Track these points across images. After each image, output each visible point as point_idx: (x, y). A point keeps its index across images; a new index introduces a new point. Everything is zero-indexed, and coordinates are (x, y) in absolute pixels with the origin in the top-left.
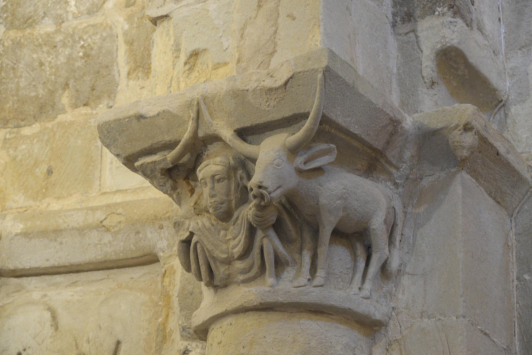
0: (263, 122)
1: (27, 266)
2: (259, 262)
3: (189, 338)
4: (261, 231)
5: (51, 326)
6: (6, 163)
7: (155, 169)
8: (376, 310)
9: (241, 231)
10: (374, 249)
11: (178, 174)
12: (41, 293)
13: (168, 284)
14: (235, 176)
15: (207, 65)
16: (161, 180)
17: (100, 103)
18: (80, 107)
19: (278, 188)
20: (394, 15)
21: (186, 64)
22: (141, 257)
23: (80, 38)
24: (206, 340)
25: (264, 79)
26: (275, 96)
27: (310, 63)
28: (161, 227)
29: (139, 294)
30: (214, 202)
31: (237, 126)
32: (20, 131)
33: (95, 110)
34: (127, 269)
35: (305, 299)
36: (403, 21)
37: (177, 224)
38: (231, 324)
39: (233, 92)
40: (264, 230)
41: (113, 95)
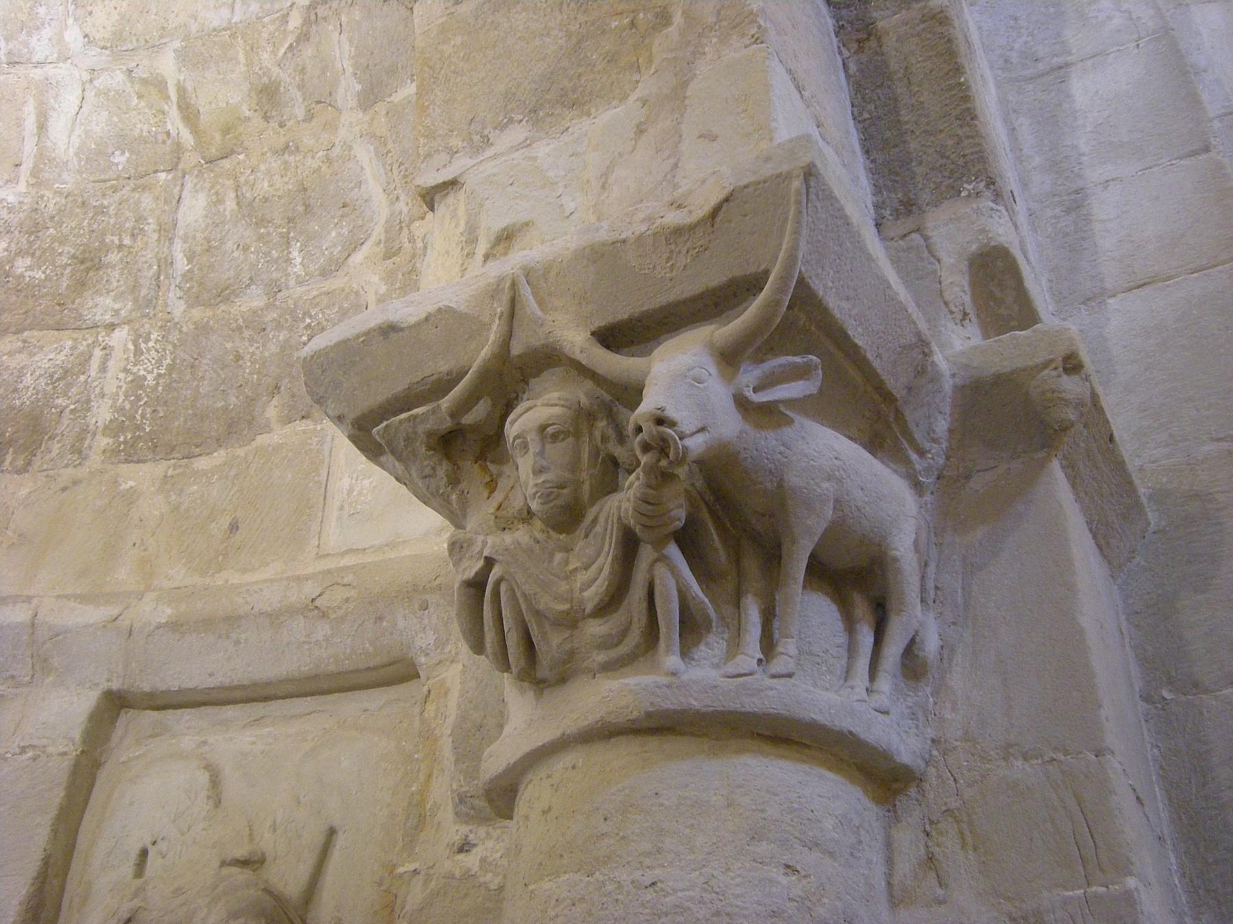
0: (658, 306)
1: (175, 685)
2: (644, 620)
5: (209, 798)
7: (416, 433)
8: (905, 745)
9: (603, 545)
14: (591, 434)
19: (698, 431)
20: (877, 206)
22: (384, 666)
23: (304, 314)
24: (511, 818)
28: (425, 607)
31: (599, 323)
35: (753, 704)
36: (897, 214)
38: (574, 767)
40: (659, 544)
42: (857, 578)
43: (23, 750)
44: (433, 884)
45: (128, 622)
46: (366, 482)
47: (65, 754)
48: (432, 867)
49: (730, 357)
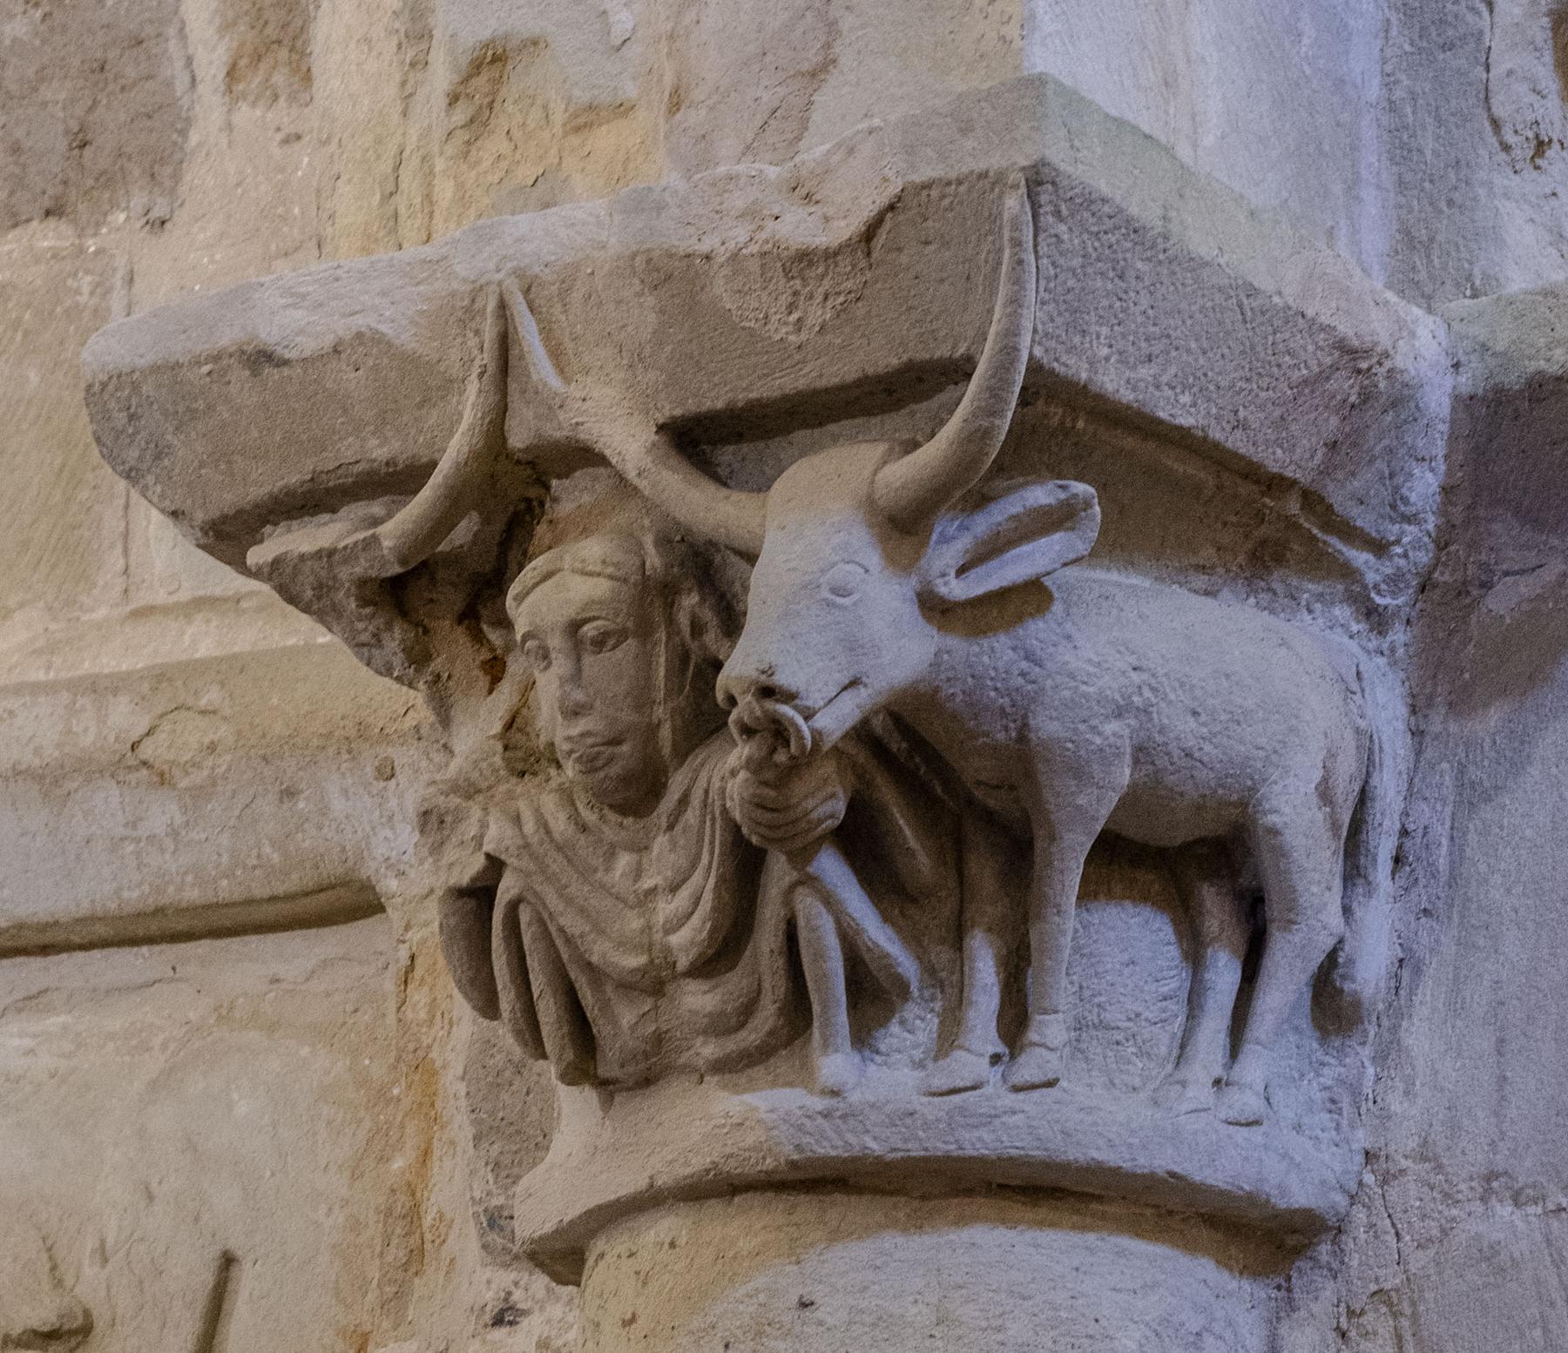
4: (783, 858)
7: (335, 578)
8: (1294, 1165)
10: (1274, 909)
11: (437, 601)
13: (423, 1015)
14: (671, 621)
15: (545, 107)
16: (360, 626)
17: (114, 205)
18: (28, 220)
21: (454, 99)
22: (307, 894)
25: (776, 211)
26: (827, 283)
27: (969, 144)
28: (387, 772)
29: (305, 1051)
30: (582, 735)
31: (669, 410)
33: (95, 235)
34: (253, 939)
35: (979, 1142)
37: (434, 819)
38: (672, 1245)
39: (649, 261)
41: (168, 170)
42: (1199, 862)
49: (903, 526)
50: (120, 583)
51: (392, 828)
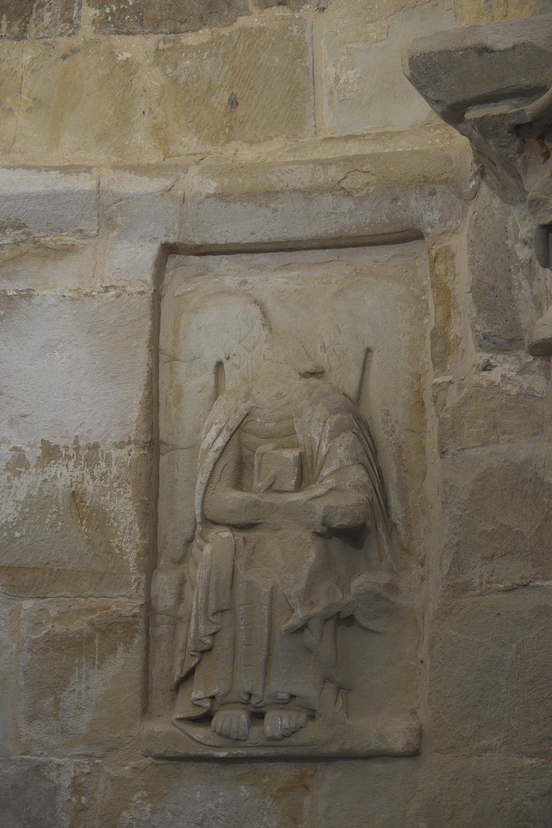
1: (222, 240)
3: (493, 349)
6: (163, 86)
7: (503, 124)
12: (236, 278)
13: (443, 272)
18: (272, 6)
22: (395, 233)
28: (433, 193)
32: (180, 39)
33: (298, 12)
34: (368, 248)
43: (107, 289)
44: (465, 390)
45: (180, 192)
46: (351, 73)
47: (142, 293)
48: (463, 380)
50: (313, 129)
51: (432, 212)
